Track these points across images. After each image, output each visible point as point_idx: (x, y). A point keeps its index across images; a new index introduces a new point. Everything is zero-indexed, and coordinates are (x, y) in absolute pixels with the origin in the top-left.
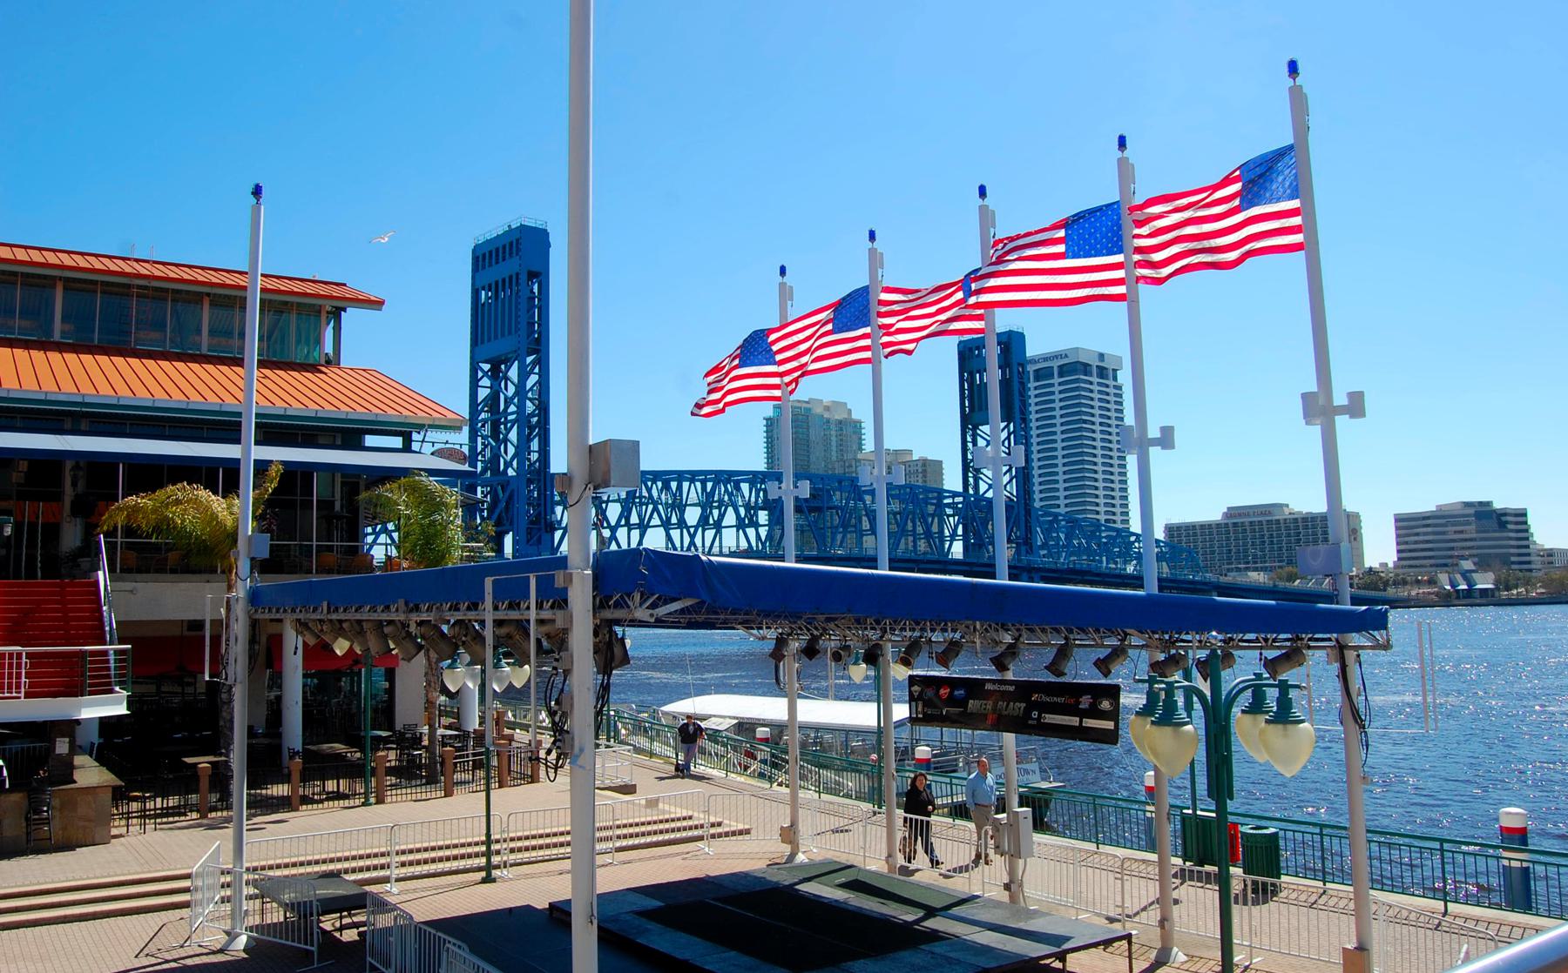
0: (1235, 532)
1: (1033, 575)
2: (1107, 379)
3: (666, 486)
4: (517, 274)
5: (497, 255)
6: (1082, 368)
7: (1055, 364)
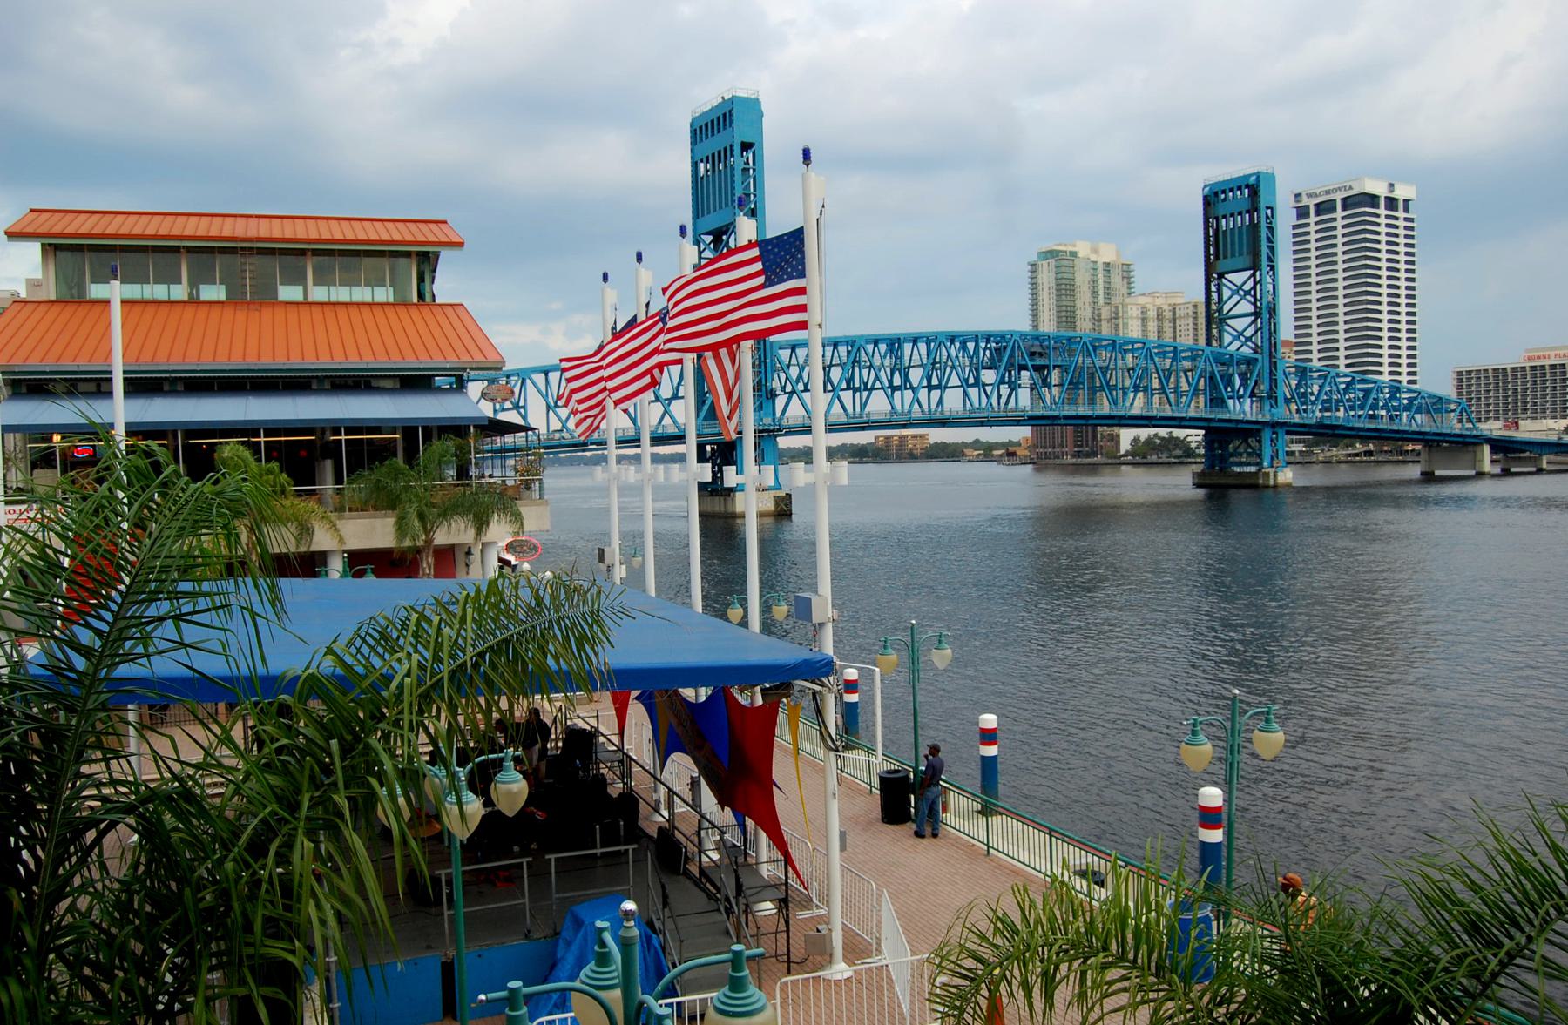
0: (1496, 378)
1: (1276, 430)
2: (1397, 210)
3: (964, 348)
4: (731, 146)
5: (713, 128)
6: (1369, 200)
7: (1338, 196)
